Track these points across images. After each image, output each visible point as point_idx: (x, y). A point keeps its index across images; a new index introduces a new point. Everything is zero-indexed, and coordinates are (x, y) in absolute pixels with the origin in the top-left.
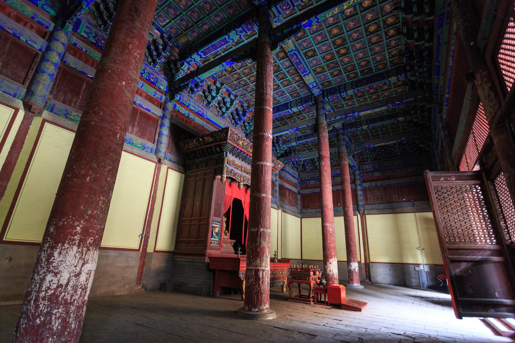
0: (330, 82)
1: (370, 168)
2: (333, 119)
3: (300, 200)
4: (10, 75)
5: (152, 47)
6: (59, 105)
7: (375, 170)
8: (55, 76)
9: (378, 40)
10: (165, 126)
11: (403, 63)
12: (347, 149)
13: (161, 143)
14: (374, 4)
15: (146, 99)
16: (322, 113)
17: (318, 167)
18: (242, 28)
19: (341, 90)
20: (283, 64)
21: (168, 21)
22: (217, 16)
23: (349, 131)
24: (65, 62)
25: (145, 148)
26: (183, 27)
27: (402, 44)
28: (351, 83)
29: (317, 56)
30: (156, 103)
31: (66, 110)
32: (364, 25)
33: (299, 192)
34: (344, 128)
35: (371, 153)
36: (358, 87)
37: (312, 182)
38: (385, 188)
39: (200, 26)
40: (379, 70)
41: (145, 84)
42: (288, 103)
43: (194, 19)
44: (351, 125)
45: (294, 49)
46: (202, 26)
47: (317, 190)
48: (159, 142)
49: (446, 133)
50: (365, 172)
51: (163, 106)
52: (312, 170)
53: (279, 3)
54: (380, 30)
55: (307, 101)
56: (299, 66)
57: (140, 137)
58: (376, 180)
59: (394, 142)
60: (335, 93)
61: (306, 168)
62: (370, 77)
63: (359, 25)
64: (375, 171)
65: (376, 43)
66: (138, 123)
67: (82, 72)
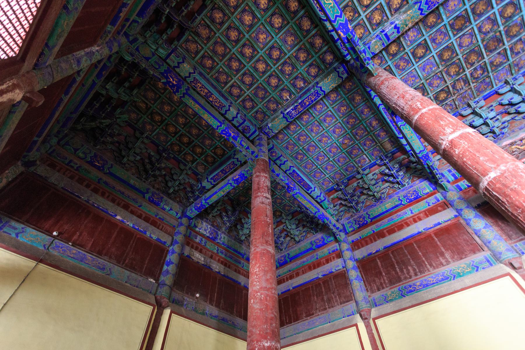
4: (345, 300)
5: (386, 178)
6: (377, 295)
8: (360, 276)
10: (470, 220)
13: (489, 242)
15: (427, 216)
21: (364, 156)
22: (362, 112)
24: (357, 259)
25: (478, 267)
26: (373, 144)
30: (439, 208)
31: (383, 295)
39: (372, 129)
41: (411, 207)
43: (365, 134)
46: (373, 127)
48: (487, 243)
51: (446, 205)
57: (461, 259)
66: (444, 246)
67: (369, 255)
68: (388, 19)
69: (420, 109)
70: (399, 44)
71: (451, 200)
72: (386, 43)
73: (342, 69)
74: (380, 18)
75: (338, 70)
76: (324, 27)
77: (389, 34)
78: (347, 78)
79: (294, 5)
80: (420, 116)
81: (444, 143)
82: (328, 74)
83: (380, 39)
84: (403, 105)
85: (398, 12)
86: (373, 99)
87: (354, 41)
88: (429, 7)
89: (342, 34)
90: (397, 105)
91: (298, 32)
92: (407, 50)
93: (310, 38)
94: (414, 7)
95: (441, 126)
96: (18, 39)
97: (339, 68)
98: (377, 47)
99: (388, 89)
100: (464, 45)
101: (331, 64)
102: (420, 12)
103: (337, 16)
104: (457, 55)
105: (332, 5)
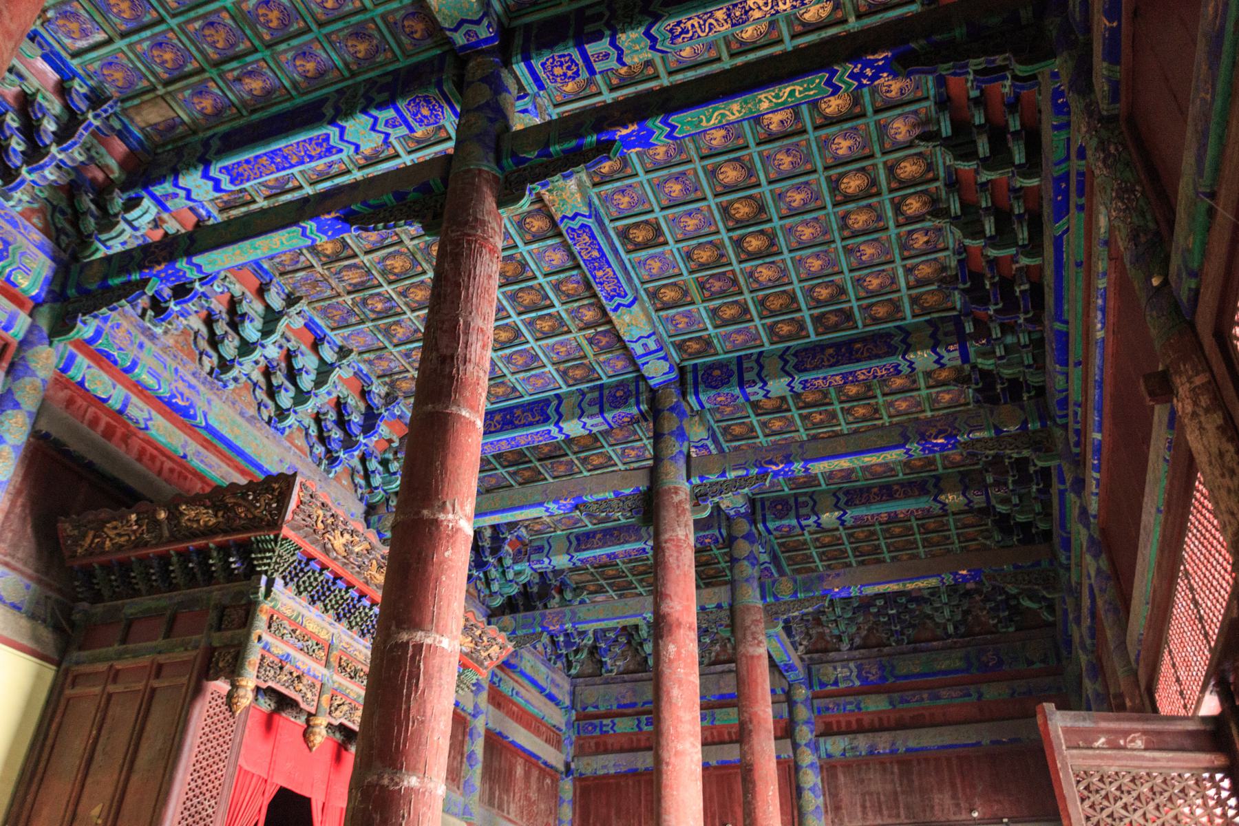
1: (846, 679)
2: (713, 478)
3: (574, 802)
7: (869, 688)
11: (954, 309)
12: (763, 597)
16: (676, 450)
17: (651, 662)
18: (398, 111)
19: (747, 376)
21: (100, 37)
22: (304, 54)
27: (946, 249)
29: (667, 248)
32: (826, 168)
33: (567, 765)
34: (753, 513)
36: (805, 370)
37: (625, 725)
38: (906, 763)
40: (876, 320)
42: (547, 402)
44: (782, 506)
45: (585, 211)
46: (238, 80)
47: (643, 761)
49: (1104, 563)
52: (627, 672)
53: (539, 55)
55: (623, 402)
56: (599, 274)
59: (933, 582)
60: (724, 382)
61: (602, 664)
71: (32, 365)
81: (450, 516)
88: (573, 230)
90: (467, 333)
96: (1197, 504)
103: (674, 128)
105: (704, 124)
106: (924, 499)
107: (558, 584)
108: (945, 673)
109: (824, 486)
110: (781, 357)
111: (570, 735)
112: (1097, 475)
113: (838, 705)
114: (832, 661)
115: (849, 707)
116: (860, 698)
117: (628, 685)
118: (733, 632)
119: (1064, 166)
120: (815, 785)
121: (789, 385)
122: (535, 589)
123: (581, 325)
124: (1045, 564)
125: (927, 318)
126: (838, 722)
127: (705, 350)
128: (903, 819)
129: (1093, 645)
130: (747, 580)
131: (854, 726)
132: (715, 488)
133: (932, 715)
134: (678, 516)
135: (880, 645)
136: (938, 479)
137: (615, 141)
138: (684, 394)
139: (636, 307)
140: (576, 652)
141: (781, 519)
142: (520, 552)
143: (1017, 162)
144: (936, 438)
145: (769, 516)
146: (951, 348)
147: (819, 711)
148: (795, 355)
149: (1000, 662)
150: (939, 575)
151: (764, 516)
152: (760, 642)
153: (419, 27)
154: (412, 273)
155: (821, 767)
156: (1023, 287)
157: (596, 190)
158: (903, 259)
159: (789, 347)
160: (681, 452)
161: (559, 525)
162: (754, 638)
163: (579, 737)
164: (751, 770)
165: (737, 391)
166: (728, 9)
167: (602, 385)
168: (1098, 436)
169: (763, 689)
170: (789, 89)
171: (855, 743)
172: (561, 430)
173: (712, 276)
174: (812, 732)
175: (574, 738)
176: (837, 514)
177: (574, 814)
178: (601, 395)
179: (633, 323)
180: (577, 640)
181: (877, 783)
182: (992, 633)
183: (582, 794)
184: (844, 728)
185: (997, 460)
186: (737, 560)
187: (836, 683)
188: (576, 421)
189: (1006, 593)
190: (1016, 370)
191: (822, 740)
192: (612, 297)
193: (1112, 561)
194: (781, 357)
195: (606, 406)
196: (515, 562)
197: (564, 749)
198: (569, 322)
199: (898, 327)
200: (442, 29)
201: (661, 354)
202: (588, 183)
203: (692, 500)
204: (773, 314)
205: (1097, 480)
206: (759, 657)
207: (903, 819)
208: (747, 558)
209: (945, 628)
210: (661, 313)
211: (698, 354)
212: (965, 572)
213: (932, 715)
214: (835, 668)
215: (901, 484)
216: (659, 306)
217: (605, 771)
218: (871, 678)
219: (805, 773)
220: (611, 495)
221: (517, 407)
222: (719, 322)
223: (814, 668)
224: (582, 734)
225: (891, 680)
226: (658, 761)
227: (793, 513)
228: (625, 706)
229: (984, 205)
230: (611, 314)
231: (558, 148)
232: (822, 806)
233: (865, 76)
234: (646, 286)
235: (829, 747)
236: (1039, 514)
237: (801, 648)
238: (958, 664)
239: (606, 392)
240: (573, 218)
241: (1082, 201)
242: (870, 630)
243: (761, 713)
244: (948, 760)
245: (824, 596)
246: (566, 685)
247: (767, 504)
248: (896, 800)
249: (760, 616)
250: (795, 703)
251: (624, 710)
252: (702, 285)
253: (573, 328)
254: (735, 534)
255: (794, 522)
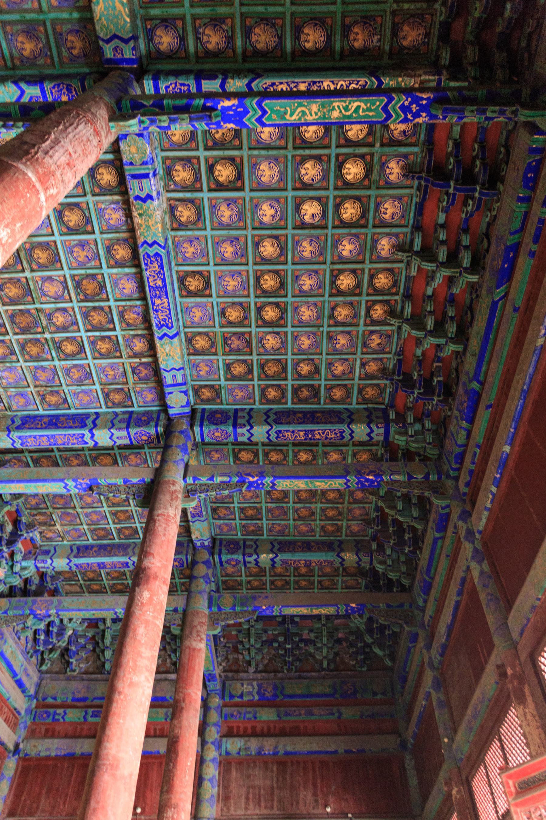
0: (217, 391)
1: (250, 693)
2: (204, 480)
3: (13, 779)
7: (264, 702)
9: (350, 320)
11: (383, 404)
12: (210, 607)
14: (363, 222)
16: (179, 457)
17: (108, 666)
18: (43, 90)
19: (240, 421)
20: (116, 283)
23: (224, 558)
27: (389, 353)
28: (267, 413)
29: (210, 300)
32: (332, 263)
33: (17, 745)
34: (213, 547)
35: (259, 650)
36: (281, 423)
37: (73, 716)
38: (283, 764)
40: (333, 401)
42: (88, 416)
44: (234, 546)
45: (161, 241)
47: (83, 746)
49: (486, 567)
50: (236, 705)
52: (86, 673)
53: (166, 79)
54: (360, 295)
55: (147, 423)
56: (158, 302)
58: (262, 735)
59: (331, 611)
60: (224, 422)
61: (68, 663)
62: (307, 411)
63: (321, 259)
64: (262, 706)
65: (344, 324)
68: (168, 191)
69: (46, 190)
70: (109, 190)
72: (129, 170)
73: (128, 54)
74: (177, 179)
75: (132, 44)
76: (238, 73)
77: (144, 181)
78: (100, 51)
79: (311, 38)
80: (34, 186)
82: (133, 15)
83: (144, 163)
84: (55, 158)
85: (168, 211)
86: (16, 83)
87: (200, 119)
88: (149, 256)
89: (227, 103)
91: (261, 9)
92: (90, 198)
93: (233, 27)
94: (163, 236)
95: (14, 221)
97: (134, 48)
98: (133, 150)
99: (85, 139)
100: (46, 284)
101: (150, 35)
102: (150, 242)
103: (264, 112)
104: (32, 270)
105: (288, 117)
106: (331, 554)
107: (52, 587)
108: (318, 696)
109: (265, 536)
110: (266, 414)
111: (26, 719)
112: (494, 489)
113: (240, 713)
114: (242, 680)
115: (248, 716)
116: (257, 709)
117: (85, 683)
118: (182, 630)
119: (517, 236)
120: (214, 776)
121: (267, 432)
122: (33, 588)
123: (131, 354)
124: (406, 606)
125: (365, 406)
126: (238, 727)
127: (214, 399)
128: (276, 811)
129: (440, 662)
130: (200, 593)
131: (249, 731)
132: (203, 488)
133: (305, 727)
134: (172, 500)
135: (276, 671)
136: (341, 542)
137: (217, 109)
138: (192, 426)
139: (176, 340)
140: (51, 651)
141: (232, 553)
142: (30, 552)
143: (464, 265)
144: (368, 475)
145: (224, 551)
146: (380, 425)
147: (226, 718)
148: (275, 414)
149: (355, 692)
150: (337, 605)
151: (220, 551)
152: (202, 639)
153: (77, 44)
154: (12, 269)
155: (220, 762)
156: (439, 379)
157: (173, 233)
158: (362, 354)
159: (271, 409)
160: (183, 460)
161: (67, 536)
162: (198, 635)
163: (34, 723)
164: (176, 742)
165: (230, 430)
166: (309, 84)
167: (132, 412)
168: (507, 449)
169: (198, 675)
170: (356, 104)
171: (249, 744)
172: (93, 435)
173: (235, 334)
174: (218, 732)
175: (29, 723)
176: (271, 556)
177: (10, 791)
178: (130, 417)
179: (171, 354)
180: (54, 640)
181: (260, 778)
182: (351, 670)
183: (22, 773)
184: (241, 732)
185: (406, 498)
186: (195, 577)
187: (241, 696)
188: (106, 431)
189: (365, 641)
190: (419, 445)
191: (224, 740)
192: (162, 326)
193: (492, 564)
194: (266, 414)
195: (132, 424)
196: (24, 558)
197: (18, 732)
198: (122, 348)
199: (346, 409)
200: (97, 37)
201: (184, 388)
202: (168, 226)
203: (184, 493)
204: (268, 378)
205: (494, 495)
206: (200, 650)
207: (276, 811)
208: (203, 577)
209: (321, 664)
210: (192, 357)
211: (208, 401)
212: (354, 605)
213: (305, 727)
214: (242, 685)
215: (317, 542)
216: (191, 351)
217: (47, 753)
218: (267, 694)
219: (208, 766)
220: (120, 482)
221: (63, 415)
222: (229, 377)
223: (228, 683)
224: (37, 720)
225: (281, 697)
226: (112, 690)
227: (241, 551)
228: (79, 700)
229: (428, 309)
230: (157, 341)
231: (170, 102)
232: (216, 795)
233: (411, 111)
234: (187, 330)
235: (229, 746)
236: (404, 573)
237: (221, 667)
238: (328, 691)
239: (134, 416)
240: (151, 245)
241: (534, 248)
242: (270, 660)
243: (193, 694)
244: (313, 763)
245: (254, 611)
246: (35, 678)
247: (224, 543)
248: (272, 794)
249: (204, 620)
250: (210, 708)
251: (78, 702)
252: (225, 341)
253: (124, 354)
254: (198, 560)
255: (241, 558)
